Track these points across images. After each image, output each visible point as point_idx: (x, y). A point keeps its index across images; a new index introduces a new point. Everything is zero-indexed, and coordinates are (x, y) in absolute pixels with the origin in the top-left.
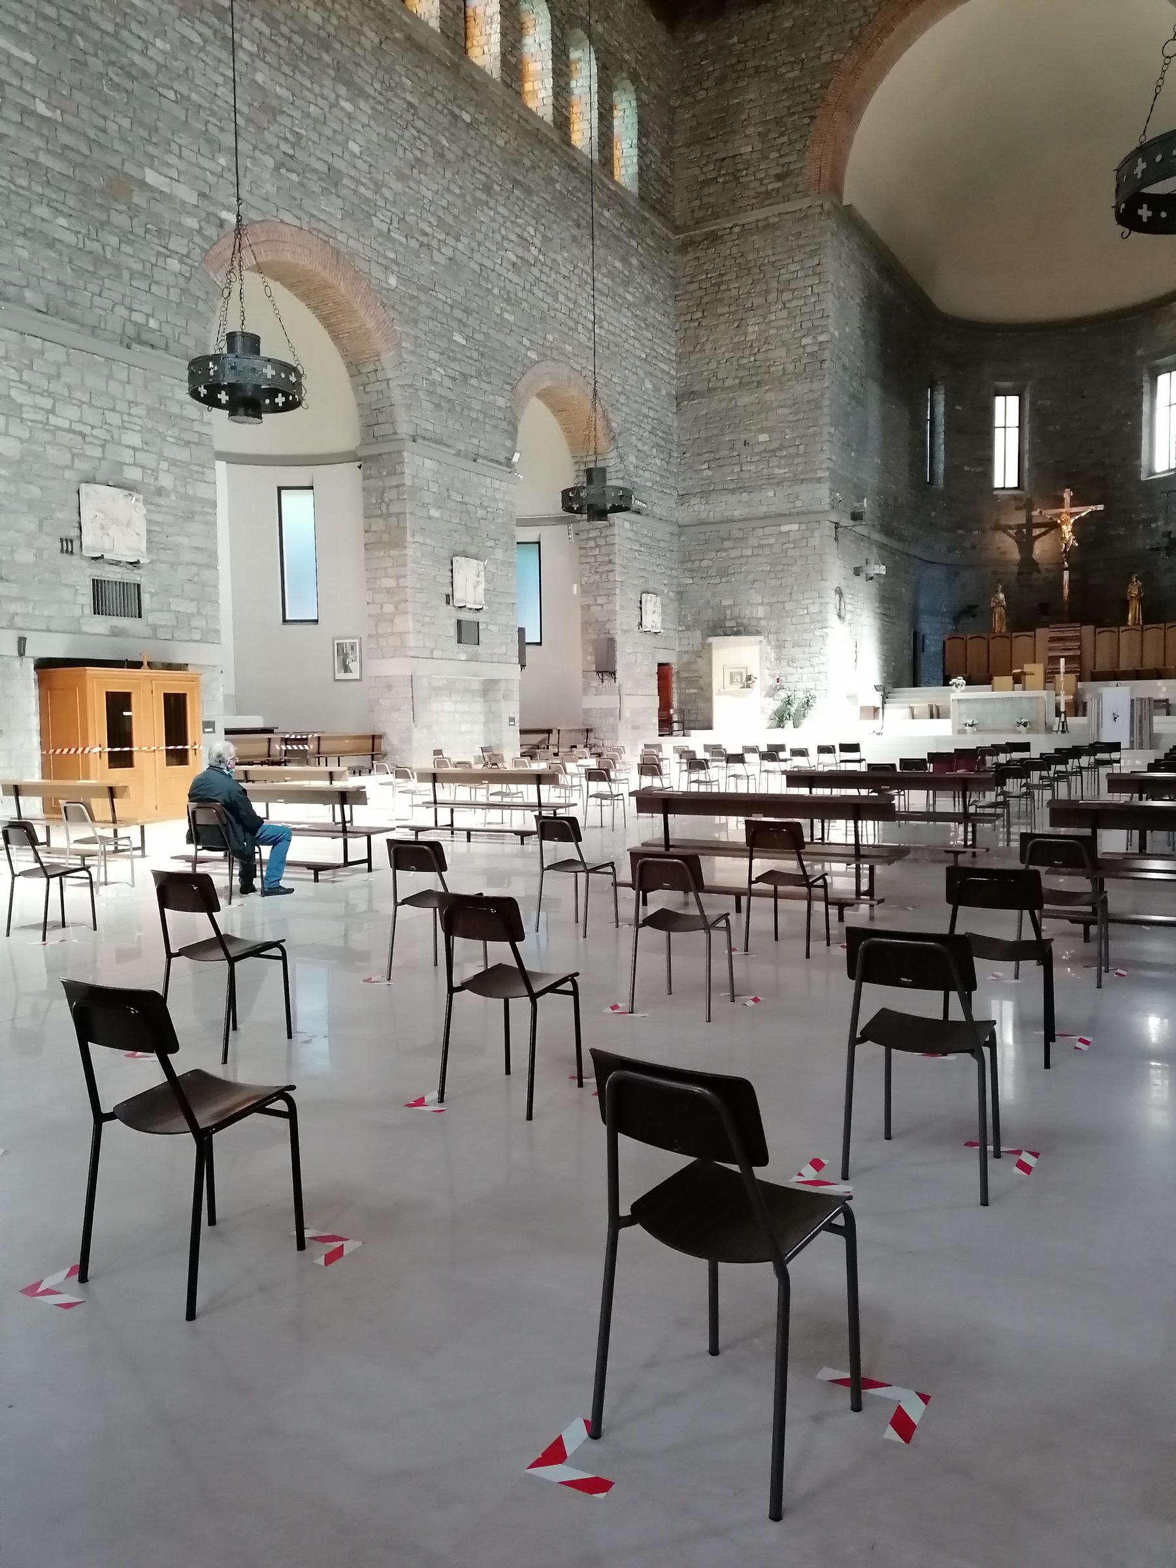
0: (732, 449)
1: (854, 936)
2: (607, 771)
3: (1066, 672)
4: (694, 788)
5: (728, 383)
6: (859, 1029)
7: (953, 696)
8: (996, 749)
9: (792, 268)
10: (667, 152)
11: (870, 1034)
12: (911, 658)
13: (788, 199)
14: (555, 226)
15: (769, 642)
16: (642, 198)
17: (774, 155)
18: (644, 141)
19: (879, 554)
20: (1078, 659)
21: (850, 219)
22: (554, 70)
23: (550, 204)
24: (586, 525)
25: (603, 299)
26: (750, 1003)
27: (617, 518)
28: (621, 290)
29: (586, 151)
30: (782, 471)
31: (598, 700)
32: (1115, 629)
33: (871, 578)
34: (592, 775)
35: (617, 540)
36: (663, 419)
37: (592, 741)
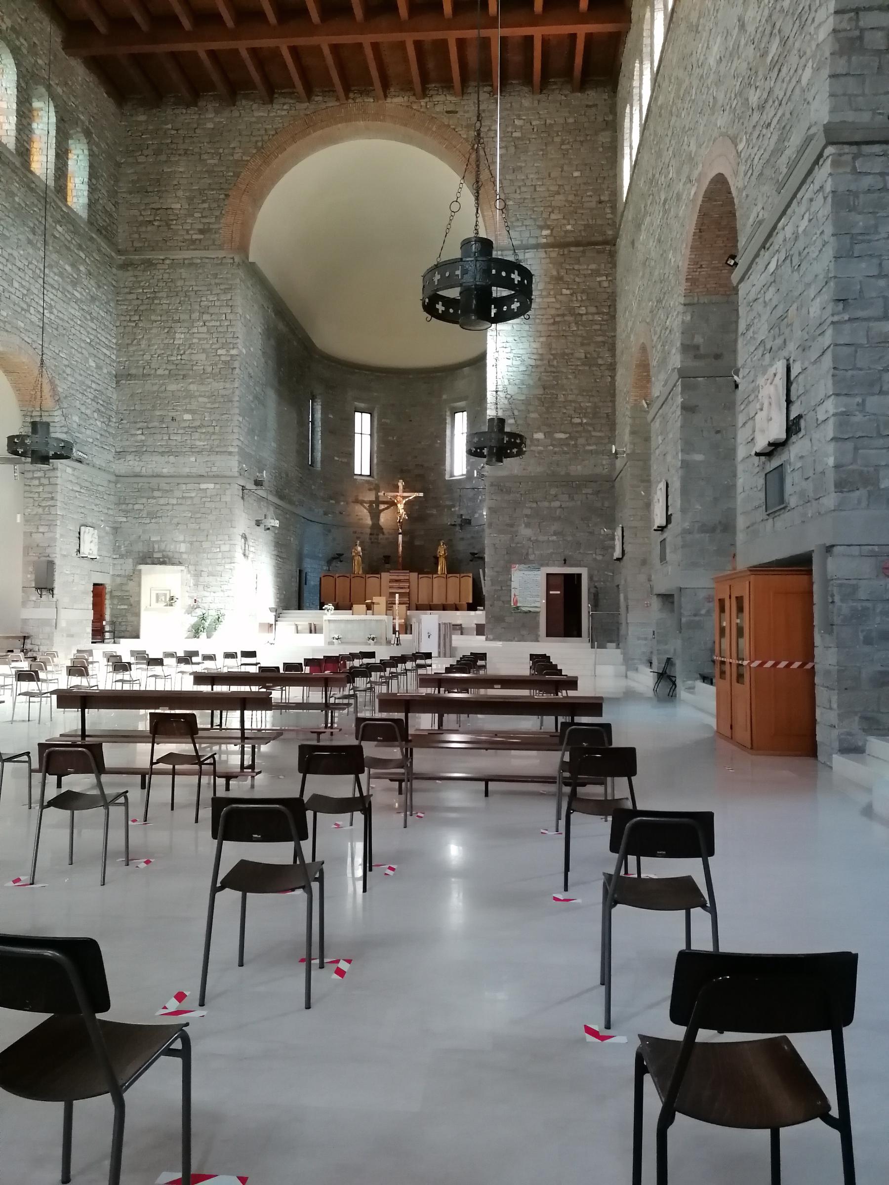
0: (162, 421)
1: (218, 803)
2: (36, 672)
3: (400, 604)
4: (118, 687)
5: (159, 372)
6: (220, 879)
7: (325, 618)
8: (353, 656)
9: (211, 298)
10: (113, 194)
11: (229, 882)
12: (297, 589)
13: (206, 248)
14: (12, 229)
15: (189, 572)
16: (90, 223)
17: (197, 215)
18: (94, 181)
19: (274, 512)
20: (408, 594)
21: (253, 271)
22: (18, 111)
23: (10, 211)
24: (29, 467)
25: (54, 291)
26: (143, 865)
27: (59, 463)
28: (70, 288)
29: (43, 178)
30: (202, 443)
31: (37, 612)
32: (430, 576)
33: (269, 529)
34: (22, 676)
35: (59, 481)
36: (104, 391)
37: (28, 646)
